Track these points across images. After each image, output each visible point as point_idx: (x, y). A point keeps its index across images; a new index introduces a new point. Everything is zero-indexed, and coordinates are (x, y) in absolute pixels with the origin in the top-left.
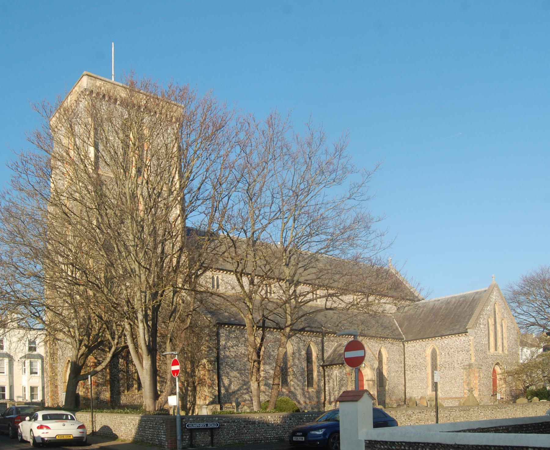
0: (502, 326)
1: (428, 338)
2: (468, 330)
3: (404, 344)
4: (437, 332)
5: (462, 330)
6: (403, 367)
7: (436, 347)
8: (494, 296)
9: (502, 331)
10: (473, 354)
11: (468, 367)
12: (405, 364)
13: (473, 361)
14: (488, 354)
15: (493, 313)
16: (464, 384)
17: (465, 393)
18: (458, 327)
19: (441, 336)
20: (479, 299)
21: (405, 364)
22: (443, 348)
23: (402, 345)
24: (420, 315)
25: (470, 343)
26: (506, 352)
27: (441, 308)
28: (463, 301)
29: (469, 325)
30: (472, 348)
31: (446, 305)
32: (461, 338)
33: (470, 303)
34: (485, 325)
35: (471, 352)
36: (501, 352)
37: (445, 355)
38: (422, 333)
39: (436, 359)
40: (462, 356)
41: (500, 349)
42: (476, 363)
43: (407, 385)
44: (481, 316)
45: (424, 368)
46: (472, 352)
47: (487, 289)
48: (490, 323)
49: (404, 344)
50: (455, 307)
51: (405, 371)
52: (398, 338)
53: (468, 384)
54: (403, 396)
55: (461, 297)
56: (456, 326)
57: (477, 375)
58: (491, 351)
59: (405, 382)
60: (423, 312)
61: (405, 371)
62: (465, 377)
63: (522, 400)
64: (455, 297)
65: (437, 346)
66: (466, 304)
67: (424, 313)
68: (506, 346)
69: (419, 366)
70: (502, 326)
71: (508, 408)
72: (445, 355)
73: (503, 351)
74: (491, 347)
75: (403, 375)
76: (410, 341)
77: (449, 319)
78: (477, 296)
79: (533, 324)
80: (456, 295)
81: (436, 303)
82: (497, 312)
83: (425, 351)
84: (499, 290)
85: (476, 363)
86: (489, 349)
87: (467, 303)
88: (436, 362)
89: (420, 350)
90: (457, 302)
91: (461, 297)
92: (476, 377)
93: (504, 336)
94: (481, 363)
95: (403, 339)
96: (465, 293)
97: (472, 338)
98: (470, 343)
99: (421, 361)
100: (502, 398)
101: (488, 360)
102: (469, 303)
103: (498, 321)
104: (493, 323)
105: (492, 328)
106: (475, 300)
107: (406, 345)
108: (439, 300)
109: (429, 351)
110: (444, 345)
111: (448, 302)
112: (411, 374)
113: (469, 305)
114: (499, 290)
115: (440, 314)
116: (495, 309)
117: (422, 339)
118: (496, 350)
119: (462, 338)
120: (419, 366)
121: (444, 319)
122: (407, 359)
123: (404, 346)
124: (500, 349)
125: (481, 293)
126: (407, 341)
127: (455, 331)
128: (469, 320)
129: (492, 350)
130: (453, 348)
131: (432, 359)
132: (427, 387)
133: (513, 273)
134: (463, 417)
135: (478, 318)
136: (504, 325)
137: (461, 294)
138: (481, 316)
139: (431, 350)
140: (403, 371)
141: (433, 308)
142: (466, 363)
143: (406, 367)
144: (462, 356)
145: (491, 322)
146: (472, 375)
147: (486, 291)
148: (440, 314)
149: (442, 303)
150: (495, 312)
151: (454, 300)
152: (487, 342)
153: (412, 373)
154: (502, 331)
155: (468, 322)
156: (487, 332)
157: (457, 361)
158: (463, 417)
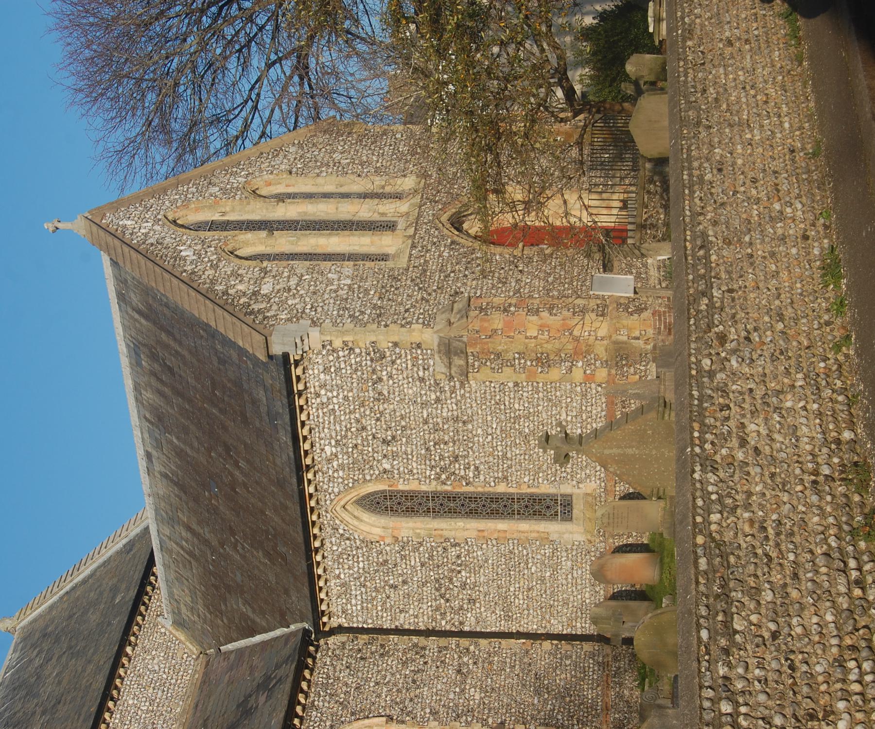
0: (281, 198)
1: (306, 526)
2: (277, 349)
3: (333, 632)
4: (281, 484)
5: (273, 378)
6: (443, 642)
7: (354, 495)
8: (140, 226)
9: (309, 196)
10: (397, 333)
11: (458, 361)
12: (428, 633)
13: (429, 337)
14: (403, 262)
15: (216, 234)
16: (541, 378)
17: (589, 378)
18: (261, 394)
19: (300, 469)
20: (146, 292)
21: (428, 633)
22: (360, 465)
23: (331, 640)
24: (206, 542)
25: (338, 343)
26: (408, 183)
27: (180, 454)
28: (153, 357)
29: (252, 344)
30: (364, 338)
31: (167, 430)
32: (313, 385)
33: (162, 328)
34: (265, 271)
35: (384, 344)
36: (404, 207)
37: (395, 455)
38: (282, 549)
39: (410, 496)
40: (403, 387)
41: (389, 209)
42: (441, 319)
43: (533, 628)
44: (220, 288)
45: (453, 552)
46: (384, 339)
47: (106, 260)
48: (260, 249)
49: (333, 632)
50: (178, 393)
51: (461, 634)
52: (304, 650)
53: (544, 361)
54: (587, 647)
55: (136, 364)
56: (255, 402)
57: (497, 321)
58: (391, 251)
59: (519, 635)
60: (194, 526)
61: (461, 634)
62: (508, 375)
63: (650, 123)
64: (137, 388)
65: (348, 489)
66: (166, 347)
67: (199, 523)
68: (379, 181)
69: (444, 571)
70: (281, 198)
71: (704, 223)
72: (395, 455)
73: (398, 196)
74: (373, 250)
75: (483, 642)
76: (315, 602)
77: (225, 428)
78: (135, 298)
79: (302, 69)
80: (129, 383)
81: (158, 467)
82: (217, 217)
83: (368, 543)
84: (115, 206)
85: (441, 319)
86: (384, 257)
87: (158, 342)
88: (425, 496)
89: (363, 559)
90: (153, 381)
91: (139, 364)
92: (508, 325)
93: (330, 188)
94: (444, 299)
95: (306, 632)
96: (122, 348)
97: (315, 333)
98: (338, 343)
99: (415, 560)
100: (625, 203)
101: (432, 266)
102: (164, 336)
103: (257, 211)
104: (263, 234)
105: (284, 242)
106: (150, 307)
107: (334, 622)
108: (149, 456)
109: (373, 526)
110: (343, 459)
111: (157, 420)
112: (480, 608)
113: (169, 333)
114: (115, 206)
115: (202, 459)
116: (199, 227)
117: (309, 552)
118: (390, 227)
119: (313, 377)
120: (444, 571)
121: (227, 449)
122: (404, 621)
123: (340, 630)
124: (389, 209)
125: (121, 281)
126: (317, 614)
127: (280, 406)
128: (233, 345)
129: (387, 243)
130: (364, 411)
131: (410, 512)
132: (545, 539)
133: (75, 145)
134: (781, 610)
135: (224, 303)
136: (281, 189)
137: (125, 361)
138: (220, 288)
139: (366, 516)
140: (464, 642)
141: (182, 487)
142: (438, 366)
143: (444, 625)
144: (403, 387)
145: (254, 243)
146: (500, 344)
147: (114, 263)
148: (202, 459)
149: (159, 446)
150: (213, 226)
151: (148, 395)
152: (348, 268)
153: (472, 601)
154: (309, 196)
155: (242, 352)
156: (301, 266)
157: (424, 405)
158: (781, 610)
